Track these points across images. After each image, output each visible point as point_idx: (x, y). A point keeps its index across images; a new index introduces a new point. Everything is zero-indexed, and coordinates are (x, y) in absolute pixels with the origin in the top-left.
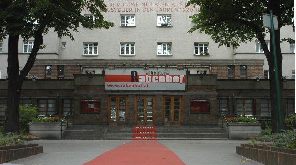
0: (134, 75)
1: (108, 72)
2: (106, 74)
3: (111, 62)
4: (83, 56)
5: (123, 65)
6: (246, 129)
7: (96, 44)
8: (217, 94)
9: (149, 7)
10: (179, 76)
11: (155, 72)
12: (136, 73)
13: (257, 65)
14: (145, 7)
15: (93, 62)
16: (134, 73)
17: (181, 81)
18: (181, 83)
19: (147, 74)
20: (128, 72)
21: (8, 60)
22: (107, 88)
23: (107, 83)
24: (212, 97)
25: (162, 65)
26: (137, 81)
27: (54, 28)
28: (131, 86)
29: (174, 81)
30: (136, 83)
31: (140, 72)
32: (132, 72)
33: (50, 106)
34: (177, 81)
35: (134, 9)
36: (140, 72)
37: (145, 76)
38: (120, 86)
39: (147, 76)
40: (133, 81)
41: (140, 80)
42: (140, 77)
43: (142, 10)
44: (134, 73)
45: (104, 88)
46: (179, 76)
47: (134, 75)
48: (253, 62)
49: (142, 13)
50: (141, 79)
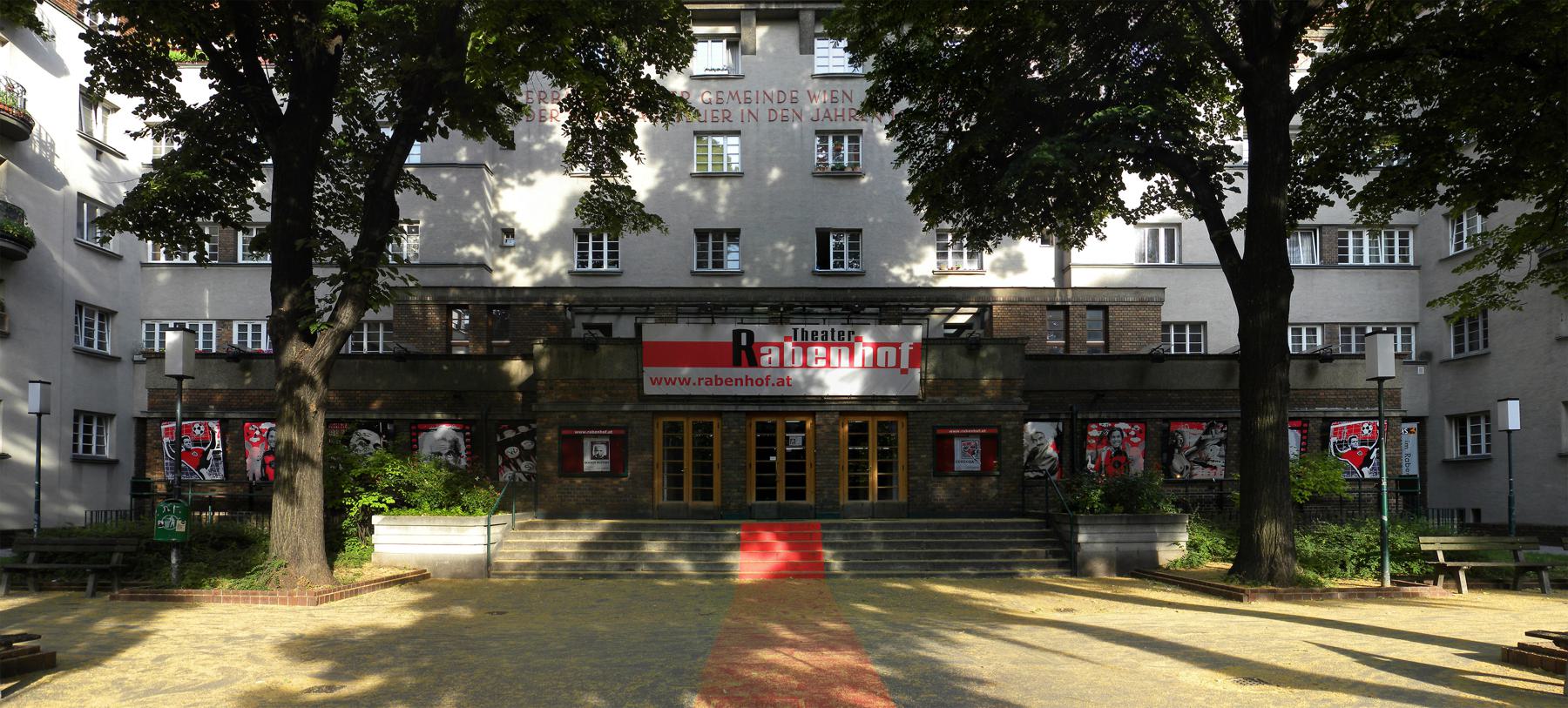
0: (744, 342)
1: (654, 332)
2: (646, 338)
3: (664, 293)
4: (693, 274)
5: (708, 306)
6: (1135, 537)
7: (855, 234)
8: (1025, 408)
9: (787, 105)
10: (897, 345)
11: (814, 333)
12: (750, 335)
13: (1143, 304)
14: (775, 105)
15: (606, 295)
16: (744, 335)
17: (905, 364)
18: (904, 372)
19: (787, 339)
20: (723, 332)
21: (1292, 288)
22: (649, 389)
23: (649, 372)
24: (1009, 420)
25: (830, 307)
26: (754, 362)
27: (1122, 195)
28: (734, 381)
29: (881, 362)
30: (753, 372)
31: (762, 332)
32: (737, 334)
33: (1270, 420)
34: (892, 362)
35: (736, 115)
36: (762, 332)
37: (781, 346)
38: (689, 379)
39: (789, 345)
40: (737, 363)
41: (764, 360)
42: (764, 350)
43: (764, 115)
44: (744, 335)
45: (641, 388)
46: (897, 345)
47: (744, 342)
48: (1130, 297)
49: (765, 126)
50: (770, 357)
